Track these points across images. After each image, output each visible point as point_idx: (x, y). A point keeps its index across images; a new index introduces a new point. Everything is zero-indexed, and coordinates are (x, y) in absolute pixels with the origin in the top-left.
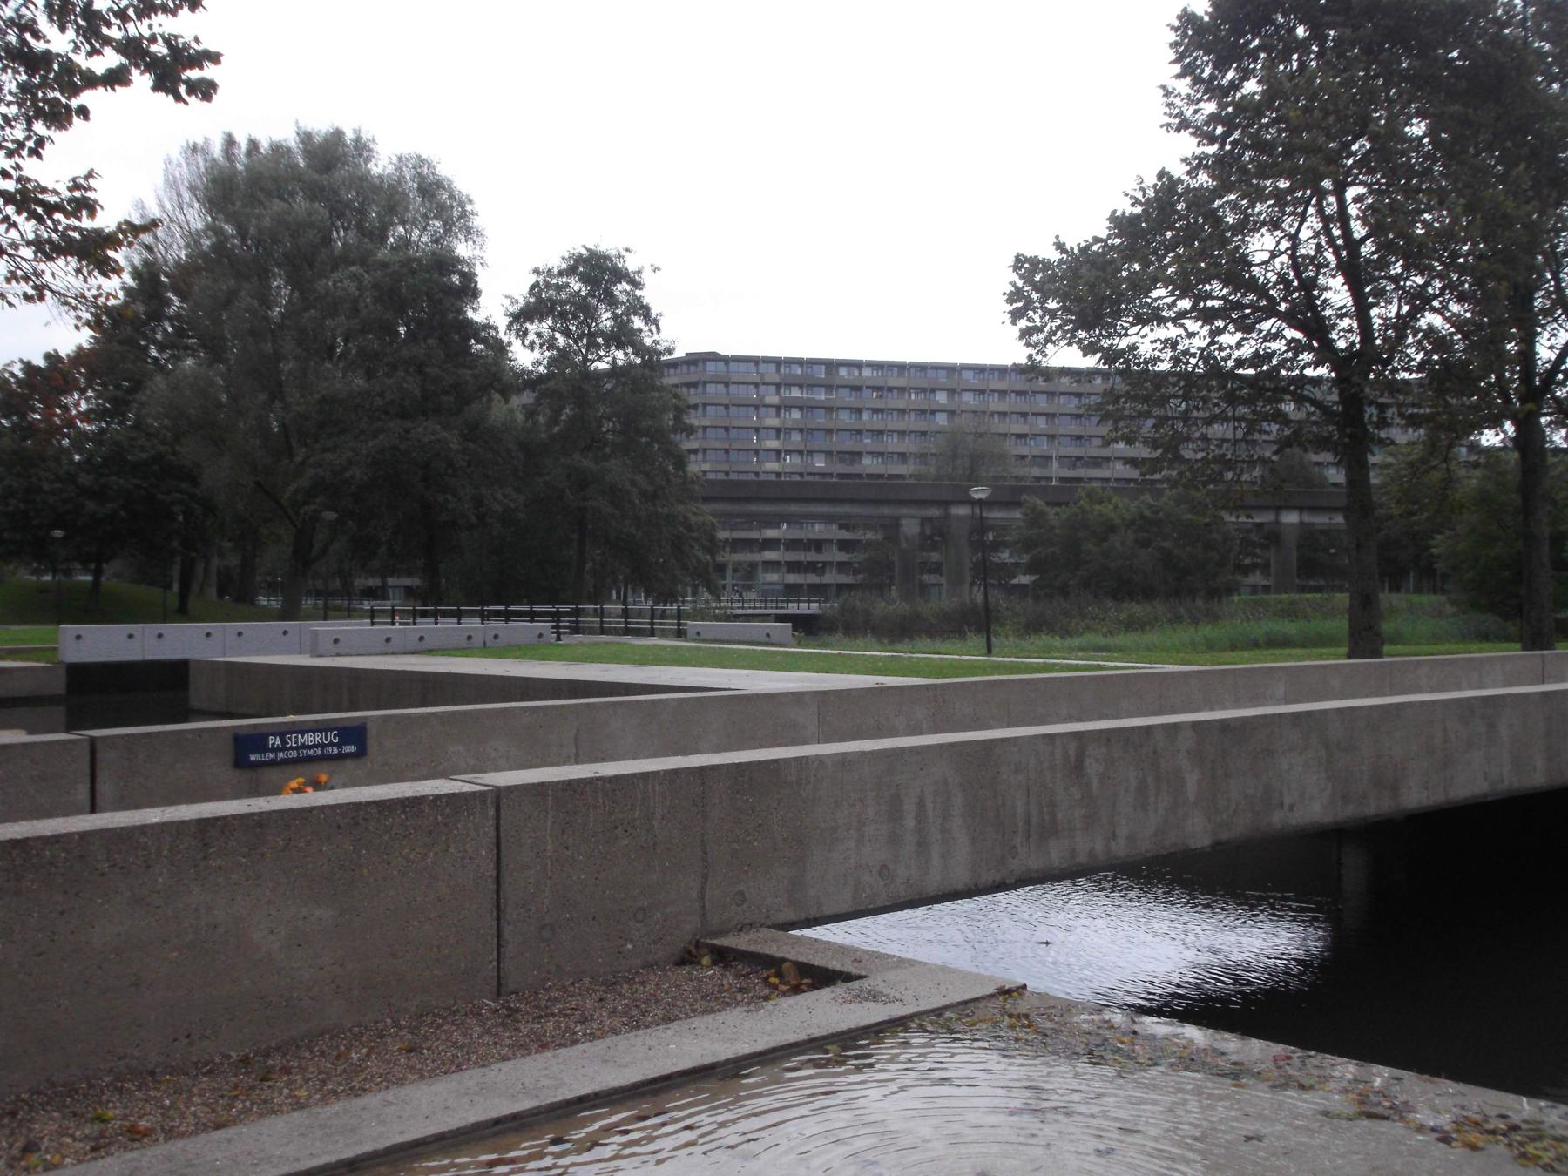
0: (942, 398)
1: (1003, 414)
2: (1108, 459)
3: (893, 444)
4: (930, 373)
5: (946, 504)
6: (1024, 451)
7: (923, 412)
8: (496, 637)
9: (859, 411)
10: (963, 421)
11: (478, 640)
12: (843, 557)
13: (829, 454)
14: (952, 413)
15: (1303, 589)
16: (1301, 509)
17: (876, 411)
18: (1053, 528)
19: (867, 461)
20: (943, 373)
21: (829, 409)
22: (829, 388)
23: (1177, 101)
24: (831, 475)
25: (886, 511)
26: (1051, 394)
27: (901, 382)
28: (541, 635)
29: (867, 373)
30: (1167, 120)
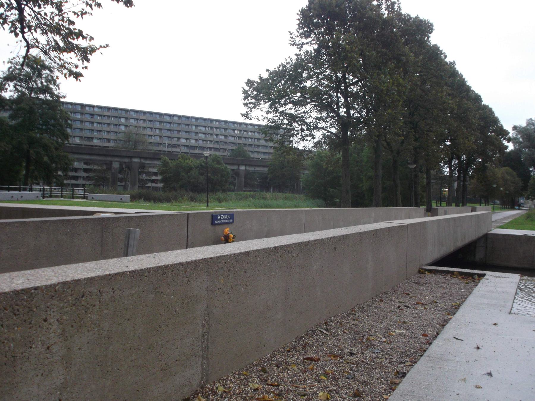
0: (123, 120)
1: (144, 128)
2: (179, 145)
3: (105, 135)
4: (119, 111)
5: (131, 157)
6: (151, 141)
7: (116, 125)
8: (22, 197)
9: (93, 123)
10: (134, 130)
11: (15, 198)
12: (85, 175)
13: (81, 137)
14: (126, 126)
15: (245, 191)
16: (246, 165)
17: (99, 123)
18: (171, 168)
19: (95, 141)
20: (123, 112)
21: (82, 122)
22: (82, 114)
23: (294, 37)
24: (82, 145)
25: (109, 159)
26: (161, 122)
27: (109, 114)
28: (37, 197)
29: (96, 109)
30: (290, 42)
